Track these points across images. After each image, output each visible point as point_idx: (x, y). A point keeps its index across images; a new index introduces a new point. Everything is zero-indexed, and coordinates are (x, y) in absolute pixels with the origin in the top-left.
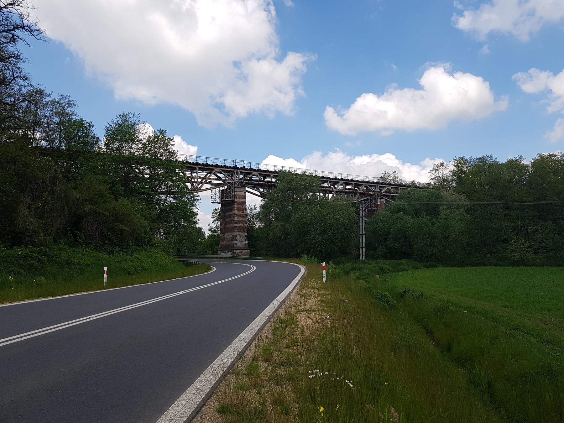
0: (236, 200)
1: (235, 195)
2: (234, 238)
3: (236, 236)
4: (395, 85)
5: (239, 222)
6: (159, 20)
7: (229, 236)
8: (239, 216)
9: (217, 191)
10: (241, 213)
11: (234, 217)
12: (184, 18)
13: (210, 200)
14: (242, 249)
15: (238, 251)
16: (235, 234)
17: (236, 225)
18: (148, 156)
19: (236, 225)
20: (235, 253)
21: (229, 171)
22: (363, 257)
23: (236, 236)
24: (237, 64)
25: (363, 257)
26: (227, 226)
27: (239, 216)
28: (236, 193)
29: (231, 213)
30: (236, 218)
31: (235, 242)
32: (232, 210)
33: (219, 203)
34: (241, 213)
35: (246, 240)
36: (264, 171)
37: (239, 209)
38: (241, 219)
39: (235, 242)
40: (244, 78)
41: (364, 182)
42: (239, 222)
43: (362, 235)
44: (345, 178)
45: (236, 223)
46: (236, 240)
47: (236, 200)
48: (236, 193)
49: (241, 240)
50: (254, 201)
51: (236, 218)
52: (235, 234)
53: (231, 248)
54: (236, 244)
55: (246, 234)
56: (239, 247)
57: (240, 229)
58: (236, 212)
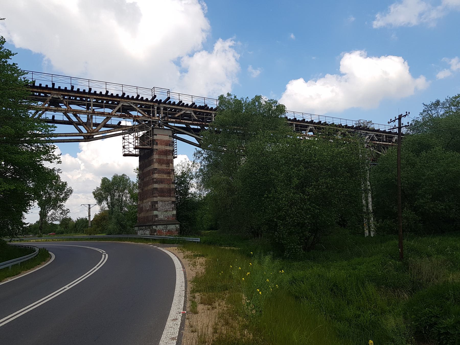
0: (155, 147)
1: (154, 140)
2: (154, 206)
3: (156, 202)
4: (343, 53)
5: (160, 181)
6: (109, 20)
7: (147, 204)
8: (160, 171)
9: (131, 137)
10: (164, 167)
11: (153, 173)
12: (129, 15)
13: (121, 152)
14: (166, 223)
15: (160, 227)
16: (155, 199)
17: (156, 186)
18: (23, 80)
19: (156, 186)
20: (155, 231)
21: (149, 106)
22: (370, 231)
23: (156, 202)
24: (178, 62)
25: (370, 231)
26: (146, 189)
27: (160, 171)
28: (155, 137)
29: (149, 168)
30: (156, 176)
31: (155, 213)
32: (151, 163)
33: (135, 155)
34: (164, 167)
35: (173, 209)
36: (200, 107)
37: (160, 162)
38: (165, 176)
39: (155, 213)
40: (184, 71)
41: (340, 126)
42: (160, 181)
43: (366, 191)
44: (316, 121)
45: (156, 182)
46: (156, 209)
47: (155, 147)
48: (155, 137)
49: (165, 210)
50: (186, 158)
51: (156, 176)
52: (155, 199)
53: (149, 222)
54: (156, 216)
55: (174, 199)
56: (161, 220)
57: (162, 193)
58: (156, 166)
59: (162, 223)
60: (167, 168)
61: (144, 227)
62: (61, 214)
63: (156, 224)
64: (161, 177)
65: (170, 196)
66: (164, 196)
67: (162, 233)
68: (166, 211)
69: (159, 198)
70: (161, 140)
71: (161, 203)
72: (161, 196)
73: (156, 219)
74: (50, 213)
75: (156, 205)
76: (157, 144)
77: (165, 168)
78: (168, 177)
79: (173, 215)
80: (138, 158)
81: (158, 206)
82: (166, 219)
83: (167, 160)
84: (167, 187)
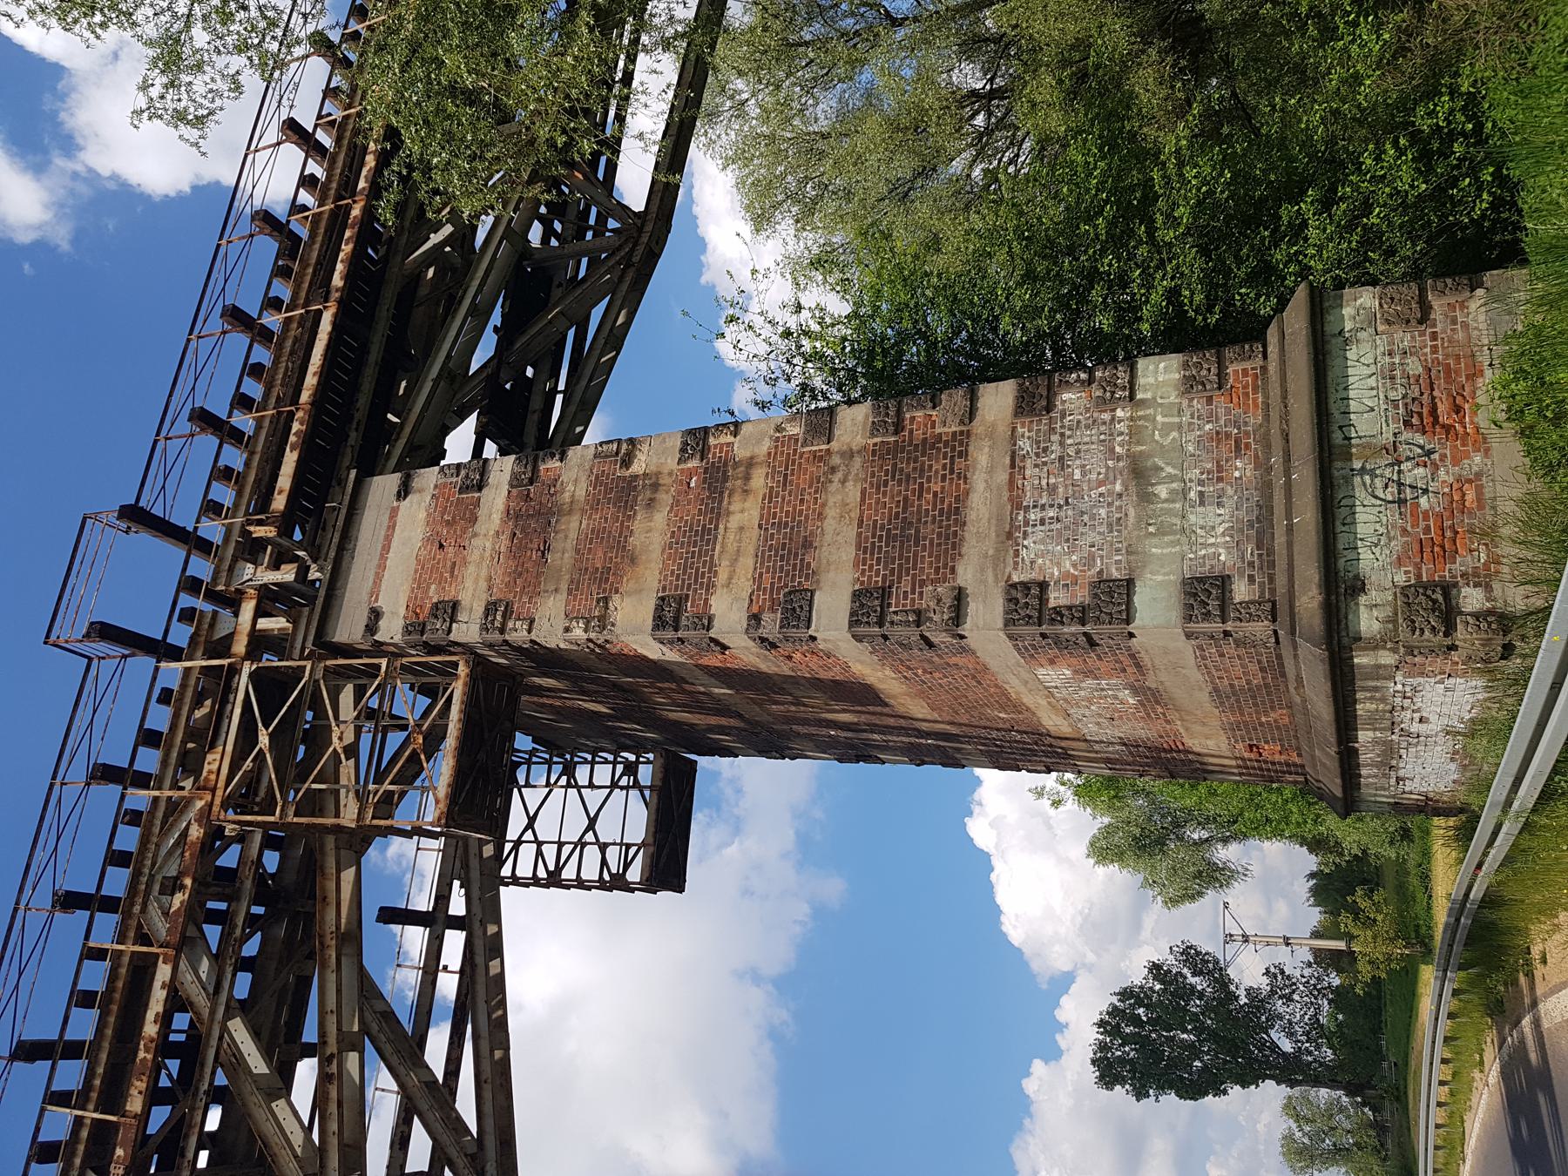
28: (391, 630)
38: (744, 515)
59: (1307, 515)
60: (665, 498)
61: (1364, 736)
62: (1288, 999)
63: (1309, 601)
64: (747, 562)
65: (959, 446)
66: (954, 514)
67: (1454, 505)
68: (1140, 473)
69: (966, 575)
70: (424, 573)
71: (1032, 546)
72: (951, 545)
73: (1241, 591)
74: (1287, 1046)
75: (1056, 598)
76: (450, 610)
77: (660, 518)
78: (759, 480)
79: (1190, 384)
80: (98, 914)
81: (1069, 582)
82: (1242, 468)
83: (594, 504)
84: (853, 492)
